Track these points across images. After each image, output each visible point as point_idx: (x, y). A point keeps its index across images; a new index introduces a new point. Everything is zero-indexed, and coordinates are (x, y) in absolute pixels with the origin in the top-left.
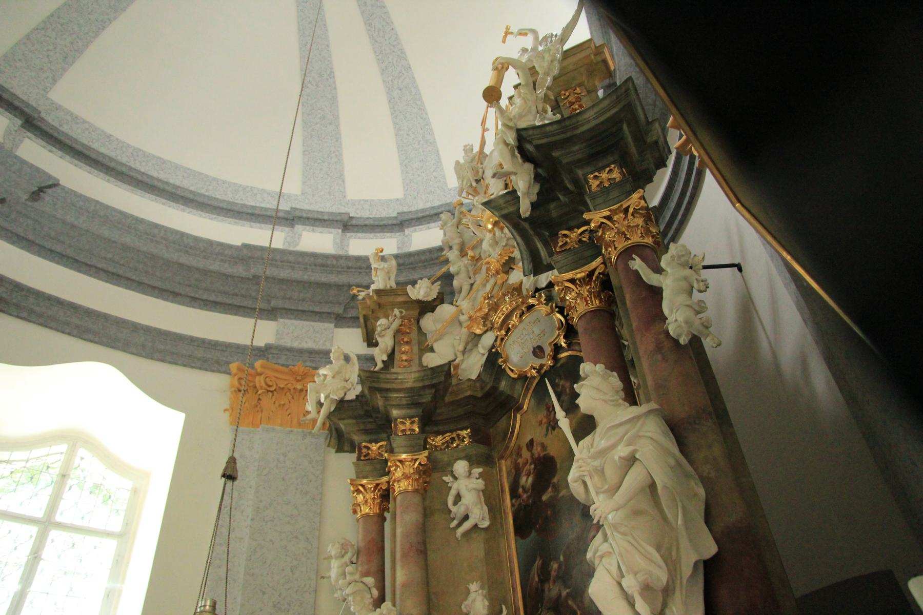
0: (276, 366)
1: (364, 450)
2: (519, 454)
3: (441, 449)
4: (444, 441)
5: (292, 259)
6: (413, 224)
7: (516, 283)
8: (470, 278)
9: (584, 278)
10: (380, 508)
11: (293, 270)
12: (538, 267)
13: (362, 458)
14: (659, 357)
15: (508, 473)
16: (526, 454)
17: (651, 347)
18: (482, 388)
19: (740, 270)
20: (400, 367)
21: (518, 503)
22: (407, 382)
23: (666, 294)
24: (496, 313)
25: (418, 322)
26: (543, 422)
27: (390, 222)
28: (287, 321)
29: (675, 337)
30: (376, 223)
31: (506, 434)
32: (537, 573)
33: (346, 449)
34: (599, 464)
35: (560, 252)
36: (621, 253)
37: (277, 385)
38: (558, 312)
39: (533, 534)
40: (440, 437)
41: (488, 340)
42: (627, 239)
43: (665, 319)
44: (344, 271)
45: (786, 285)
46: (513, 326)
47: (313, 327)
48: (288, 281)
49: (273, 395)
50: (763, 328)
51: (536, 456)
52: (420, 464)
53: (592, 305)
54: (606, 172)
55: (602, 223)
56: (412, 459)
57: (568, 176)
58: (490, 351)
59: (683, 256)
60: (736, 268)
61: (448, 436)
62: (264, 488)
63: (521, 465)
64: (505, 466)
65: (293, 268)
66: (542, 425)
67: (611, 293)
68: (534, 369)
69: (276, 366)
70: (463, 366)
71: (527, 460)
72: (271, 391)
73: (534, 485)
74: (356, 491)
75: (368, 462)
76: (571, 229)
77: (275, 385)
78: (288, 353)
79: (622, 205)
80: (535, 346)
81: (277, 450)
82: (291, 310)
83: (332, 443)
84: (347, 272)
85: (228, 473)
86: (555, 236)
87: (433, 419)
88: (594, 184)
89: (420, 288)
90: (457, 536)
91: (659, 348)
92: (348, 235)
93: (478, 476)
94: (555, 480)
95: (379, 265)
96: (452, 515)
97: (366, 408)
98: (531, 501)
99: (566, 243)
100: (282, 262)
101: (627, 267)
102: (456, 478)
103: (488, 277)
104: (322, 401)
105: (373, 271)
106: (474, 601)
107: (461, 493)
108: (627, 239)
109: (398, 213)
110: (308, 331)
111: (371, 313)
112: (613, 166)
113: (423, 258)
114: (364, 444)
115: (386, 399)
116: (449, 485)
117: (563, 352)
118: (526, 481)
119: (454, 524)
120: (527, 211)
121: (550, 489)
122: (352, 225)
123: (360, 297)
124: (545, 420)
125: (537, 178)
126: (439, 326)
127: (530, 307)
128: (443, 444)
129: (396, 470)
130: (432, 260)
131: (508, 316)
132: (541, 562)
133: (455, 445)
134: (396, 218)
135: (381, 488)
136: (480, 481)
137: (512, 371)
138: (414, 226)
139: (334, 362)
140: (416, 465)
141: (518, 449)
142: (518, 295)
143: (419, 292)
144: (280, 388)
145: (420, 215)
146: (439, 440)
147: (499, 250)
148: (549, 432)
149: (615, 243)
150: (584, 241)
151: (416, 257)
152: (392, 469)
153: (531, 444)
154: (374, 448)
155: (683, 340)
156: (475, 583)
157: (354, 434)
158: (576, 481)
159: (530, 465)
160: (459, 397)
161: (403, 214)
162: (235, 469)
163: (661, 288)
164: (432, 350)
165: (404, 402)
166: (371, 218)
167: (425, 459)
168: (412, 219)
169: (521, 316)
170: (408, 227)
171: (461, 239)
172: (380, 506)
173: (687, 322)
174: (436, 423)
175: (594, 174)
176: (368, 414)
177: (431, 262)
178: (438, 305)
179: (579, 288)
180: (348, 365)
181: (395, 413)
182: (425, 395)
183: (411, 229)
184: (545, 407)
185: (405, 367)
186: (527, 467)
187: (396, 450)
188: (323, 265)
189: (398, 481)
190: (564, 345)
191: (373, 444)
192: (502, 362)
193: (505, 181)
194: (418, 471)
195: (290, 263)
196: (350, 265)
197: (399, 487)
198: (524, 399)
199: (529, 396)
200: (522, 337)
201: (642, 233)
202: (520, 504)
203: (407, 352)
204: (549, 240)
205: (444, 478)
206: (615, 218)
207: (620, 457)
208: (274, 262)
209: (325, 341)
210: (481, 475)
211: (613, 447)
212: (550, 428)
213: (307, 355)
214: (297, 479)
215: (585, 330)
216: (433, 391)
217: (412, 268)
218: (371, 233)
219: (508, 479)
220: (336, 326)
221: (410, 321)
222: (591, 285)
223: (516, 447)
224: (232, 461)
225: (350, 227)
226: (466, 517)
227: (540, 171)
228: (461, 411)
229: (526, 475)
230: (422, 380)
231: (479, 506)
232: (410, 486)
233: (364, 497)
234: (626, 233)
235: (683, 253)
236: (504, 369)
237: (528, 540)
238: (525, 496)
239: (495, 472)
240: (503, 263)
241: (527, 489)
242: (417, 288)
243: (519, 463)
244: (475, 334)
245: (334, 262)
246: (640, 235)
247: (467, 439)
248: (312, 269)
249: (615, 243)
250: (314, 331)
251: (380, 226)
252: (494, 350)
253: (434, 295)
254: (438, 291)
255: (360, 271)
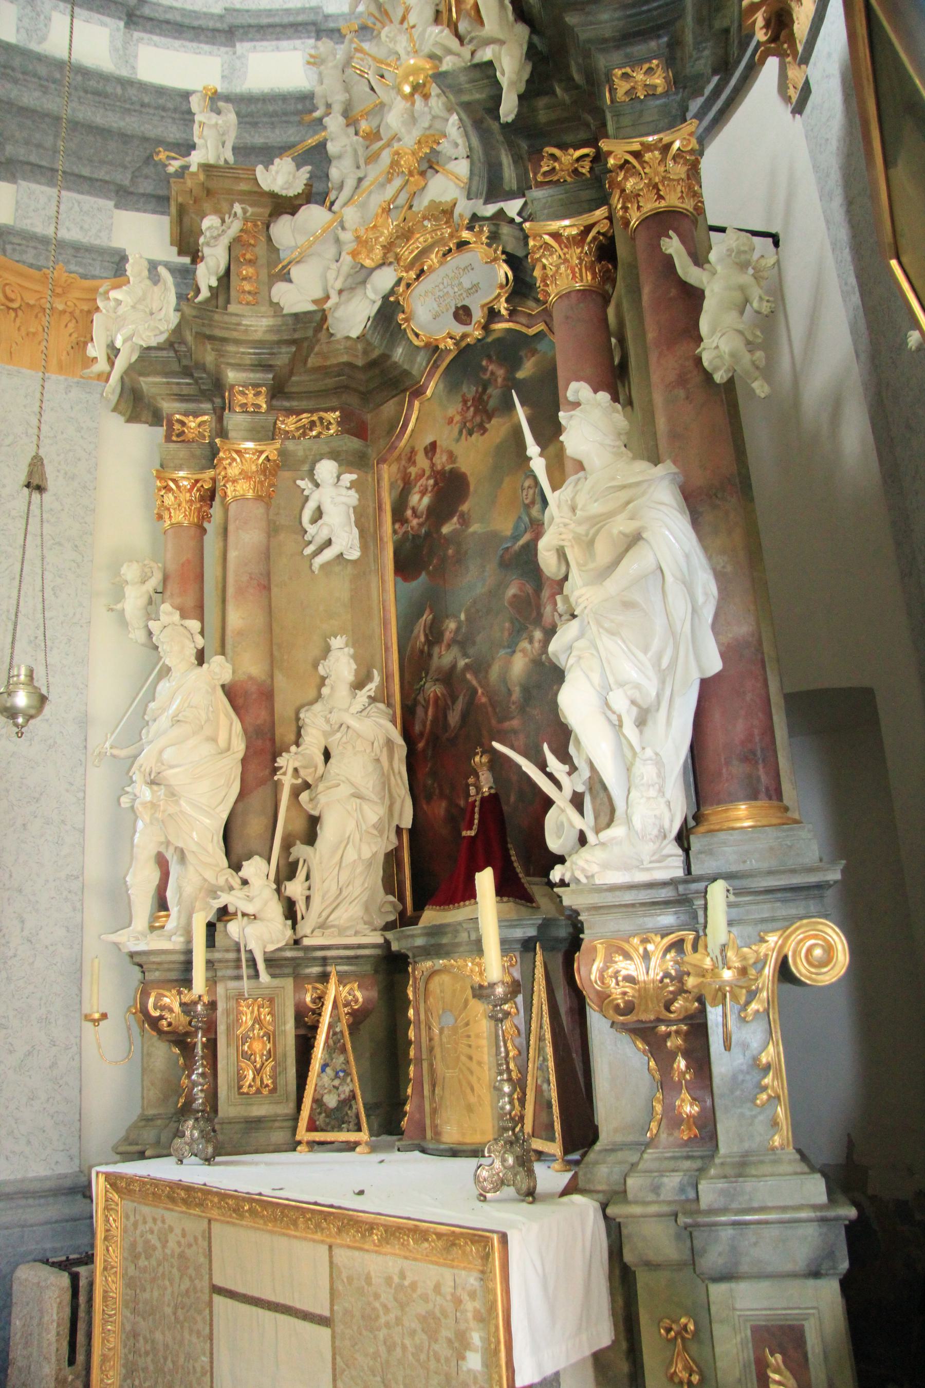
0: (20, 265)
1: (177, 426)
2: (411, 460)
3: (294, 437)
4: (299, 424)
5: (42, 71)
6: (250, 36)
7: (446, 202)
8: (358, 167)
9: (574, 237)
10: (198, 517)
11: (45, 93)
12: (494, 191)
13: (174, 438)
14: (681, 393)
15: (392, 485)
16: (422, 462)
17: (672, 376)
18: (365, 352)
19: (776, 244)
20: (240, 303)
21: (403, 530)
22: (256, 331)
23: (709, 305)
24: (406, 244)
25: (268, 227)
26: (455, 421)
27: (211, 24)
28: (34, 186)
29: (709, 369)
30: (187, 21)
31: (394, 427)
32: (424, 630)
33: (143, 419)
34: (583, 532)
35: (541, 182)
36: (647, 218)
37: (22, 299)
38: (505, 261)
39: (423, 576)
40: (293, 419)
41: (385, 279)
42: (660, 197)
43: (700, 339)
44: (135, 111)
45: (845, 295)
46: (430, 267)
47: (79, 203)
48: (34, 111)
49: (17, 316)
50: (789, 337)
51: (439, 467)
52: (267, 459)
53: (582, 280)
54: (644, 70)
55: (626, 162)
56: (257, 451)
57: (580, 61)
58: (385, 298)
59: (745, 252)
60: (770, 240)
61: (305, 418)
62: (8, 466)
63: (413, 477)
64: (388, 473)
65: (45, 90)
66: (453, 425)
67: (610, 266)
68: (451, 338)
69: (21, 267)
70: (339, 314)
71: (424, 471)
72: (15, 310)
73: (430, 510)
74: (165, 488)
75: (184, 445)
76: (563, 147)
77: (19, 299)
78: (40, 246)
79: (661, 140)
80: (459, 305)
81: (25, 406)
82: (40, 167)
83: (120, 408)
84: (141, 112)
85: (35, 481)
86: (536, 154)
87: (286, 390)
88: (622, 87)
89: (277, 172)
90: (313, 568)
91: (682, 380)
92: (136, 35)
93: (349, 485)
94: (465, 507)
95: (209, 119)
96: (308, 537)
97: (185, 362)
98: (423, 531)
99: (554, 169)
100: (24, 73)
101: (656, 247)
102: (317, 485)
103: (392, 174)
104: (118, 344)
105: (196, 126)
106: (337, 660)
107: (322, 508)
108: (660, 197)
109: (225, 9)
110: (71, 209)
111: (191, 202)
112: (655, 62)
113: (271, 108)
114: (178, 416)
115: (220, 354)
116: (306, 493)
117: (499, 322)
118: (420, 501)
119: (309, 550)
120: (511, 112)
121: (455, 519)
122: (142, 17)
123: (171, 170)
124: (458, 418)
125: (531, 53)
126: (301, 240)
127: (462, 245)
128: (298, 429)
129: (230, 464)
130: (285, 114)
131: (424, 252)
132: (431, 616)
133: (314, 433)
134: (221, 17)
135: (202, 486)
136: (352, 492)
137: (417, 335)
138: (252, 40)
139: (131, 279)
140: (260, 461)
141: (411, 452)
142: (446, 223)
143: (275, 179)
144: (28, 305)
145: (265, 21)
146: (289, 424)
147: (416, 133)
148: (463, 437)
149: (639, 199)
150: (583, 174)
151: (260, 105)
152: (226, 462)
153: (432, 448)
154: (193, 425)
155: (719, 377)
156: (338, 637)
157: (163, 399)
158: (549, 550)
159: (428, 478)
160: (328, 363)
161: (235, 14)
162: (43, 475)
163: (703, 292)
164: (286, 277)
165: (248, 362)
166: (176, 9)
167: (275, 452)
168: (250, 26)
169: (444, 255)
170: (241, 40)
171: (347, 95)
172: (199, 512)
173: (733, 355)
174: (288, 396)
175: (624, 71)
176: (187, 372)
177: (284, 118)
178: (301, 205)
179: (565, 250)
180: (156, 289)
181: (232, 376)
182: (280, 353)
183: (247, 45)
184: (461, 399)
185: (248, 304)
186: (423, 481)
187: (232, 434)
188: (97, 93)
189: (234, 481)
190: (504, 312)
191: (191, 418)
192: (403, 319)
193: (437, 5)
194: (264, 471)
195: (40, 78)
196: (146, 100)
197: (235, 490)
198: (428, 380)
199: (437, 375)
200: (441, 286)
201: (682, 192)
202: (406, 533)
203: (251, 278)
204: (525, 156)
205: (299, 482)
206: (648, 156)
207: (620, 532)
208: (9, 71)
209: (100, 231)
210: (353, 485)
211: (611, 515)
212: (464, 431)
213: (70, 251)
214: (58, 455)
215: (567, 318)
216: (294, 349)
217: (249, 123)
218: (175, 38)
219: (390, 493)
220: (117, 206)
221: (256, 225)
222: (583, 248)
223: (408, 449)
224: (37, 464)
225: (140, 20)
226: (329, 543)
227: (536, 39)
228: (330, 382)
229: (420, 492)
230: (278, 331)
231: (347, 529)
232: (251, 491)
233: (176, 498)
234: (661, 187)
235: (746, 248)
236: (405, 330)
237: (414, 584)
238: (415, 522)
239: (370, 479)
240: (421, 157)
241: (418, 513)
242: (273, 173)
243: (410, 473)
244: (362, 266)
245: (119, 91)
246: (680, 195)
247: (334, 426)
248: (79, 98)
249: (639, 199)
250: (81, 211)
251: (194, 28)
252: (392, 299)
253: (298, 187)
254: (305, 182)
255: (163, 114)
